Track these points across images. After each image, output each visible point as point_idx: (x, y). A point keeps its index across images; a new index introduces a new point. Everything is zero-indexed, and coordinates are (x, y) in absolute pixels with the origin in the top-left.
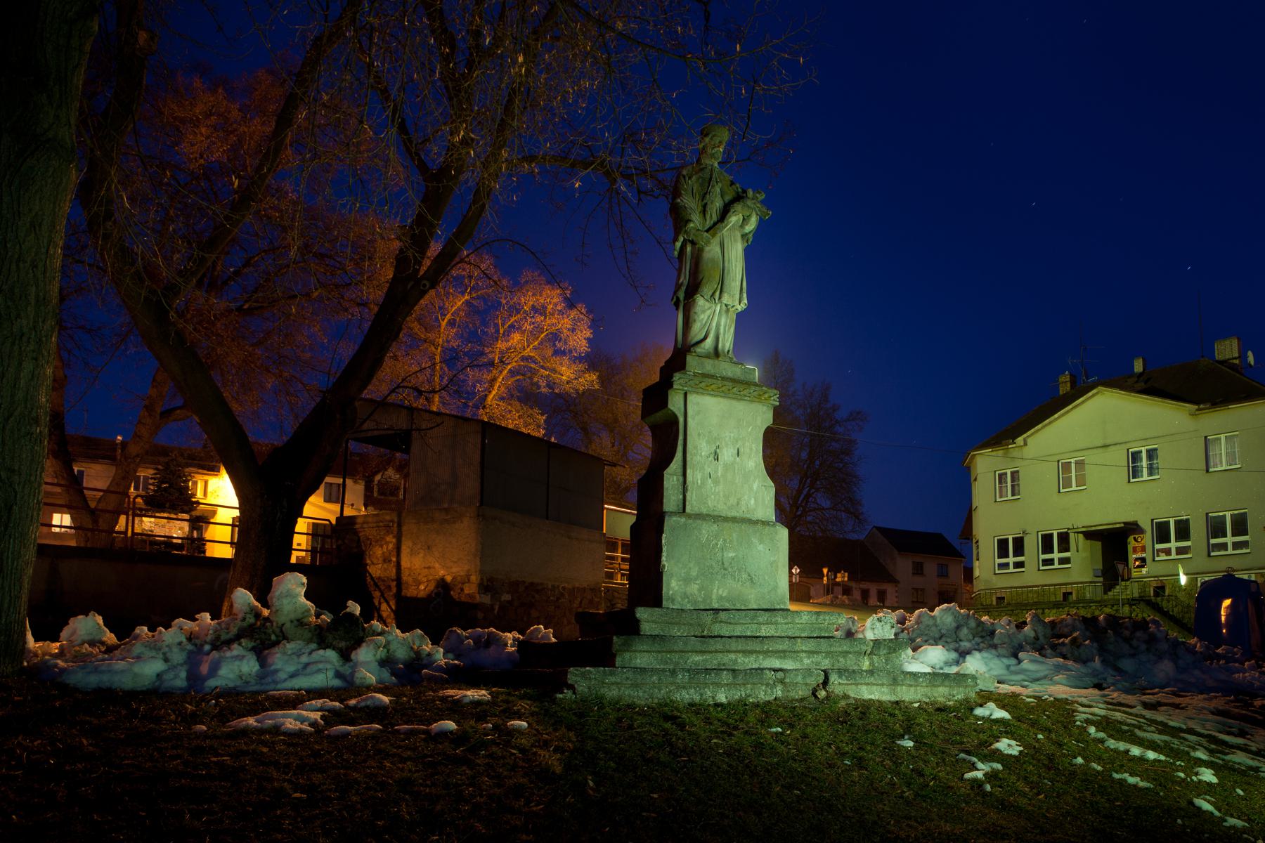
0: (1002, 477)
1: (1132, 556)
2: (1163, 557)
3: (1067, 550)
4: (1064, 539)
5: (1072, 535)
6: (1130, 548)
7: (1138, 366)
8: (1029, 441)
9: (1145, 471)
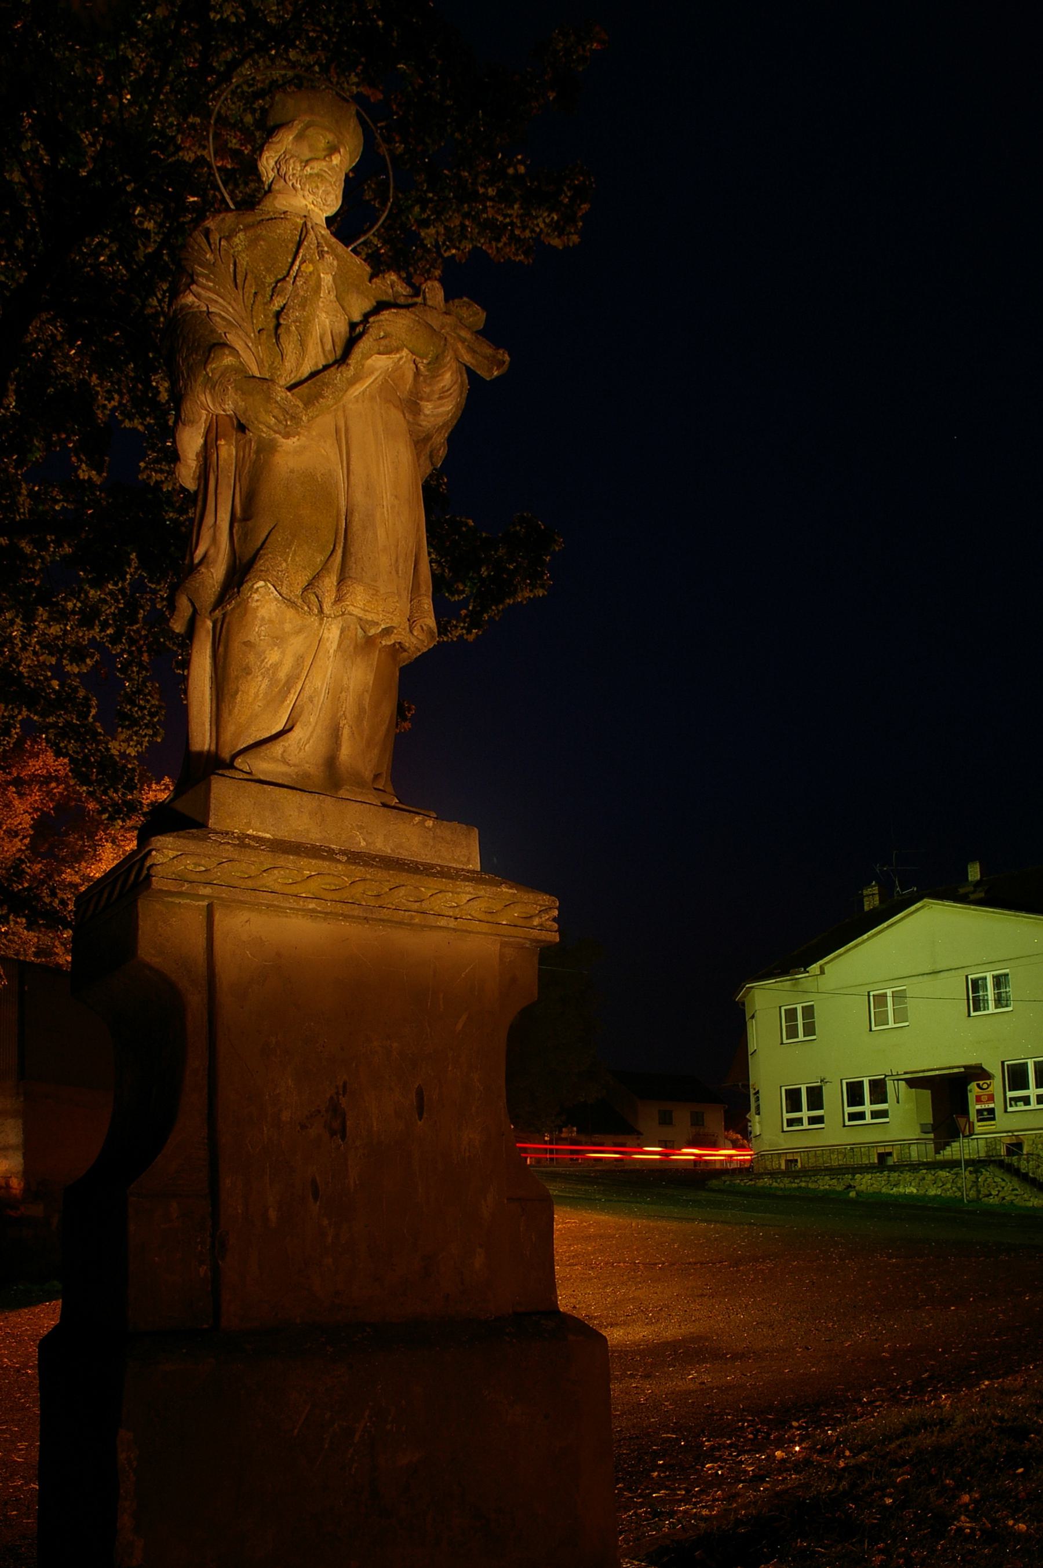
0: (791, 1014)
1: (974, 1107)
2: (1021, 1107)
3: (884, 1101)
4: (879, 1090)
5: (890, 1084)
6: (971, 1097)
7: (974, 872)
8: (826, 968)
9: (991, 1004)
